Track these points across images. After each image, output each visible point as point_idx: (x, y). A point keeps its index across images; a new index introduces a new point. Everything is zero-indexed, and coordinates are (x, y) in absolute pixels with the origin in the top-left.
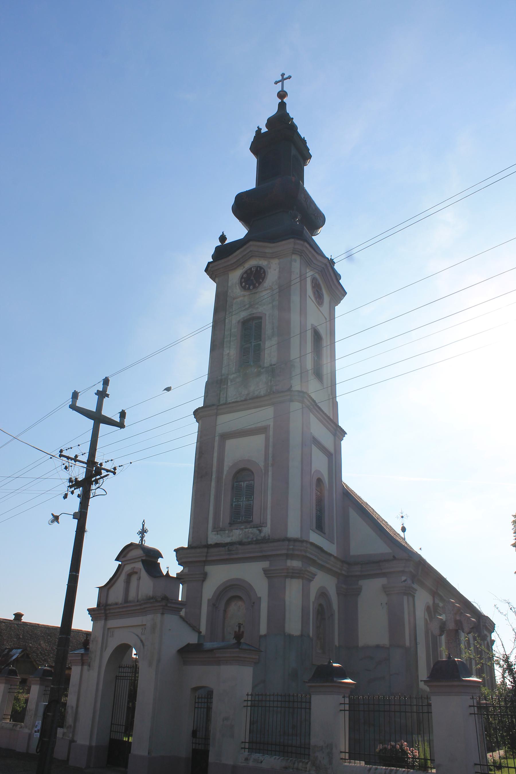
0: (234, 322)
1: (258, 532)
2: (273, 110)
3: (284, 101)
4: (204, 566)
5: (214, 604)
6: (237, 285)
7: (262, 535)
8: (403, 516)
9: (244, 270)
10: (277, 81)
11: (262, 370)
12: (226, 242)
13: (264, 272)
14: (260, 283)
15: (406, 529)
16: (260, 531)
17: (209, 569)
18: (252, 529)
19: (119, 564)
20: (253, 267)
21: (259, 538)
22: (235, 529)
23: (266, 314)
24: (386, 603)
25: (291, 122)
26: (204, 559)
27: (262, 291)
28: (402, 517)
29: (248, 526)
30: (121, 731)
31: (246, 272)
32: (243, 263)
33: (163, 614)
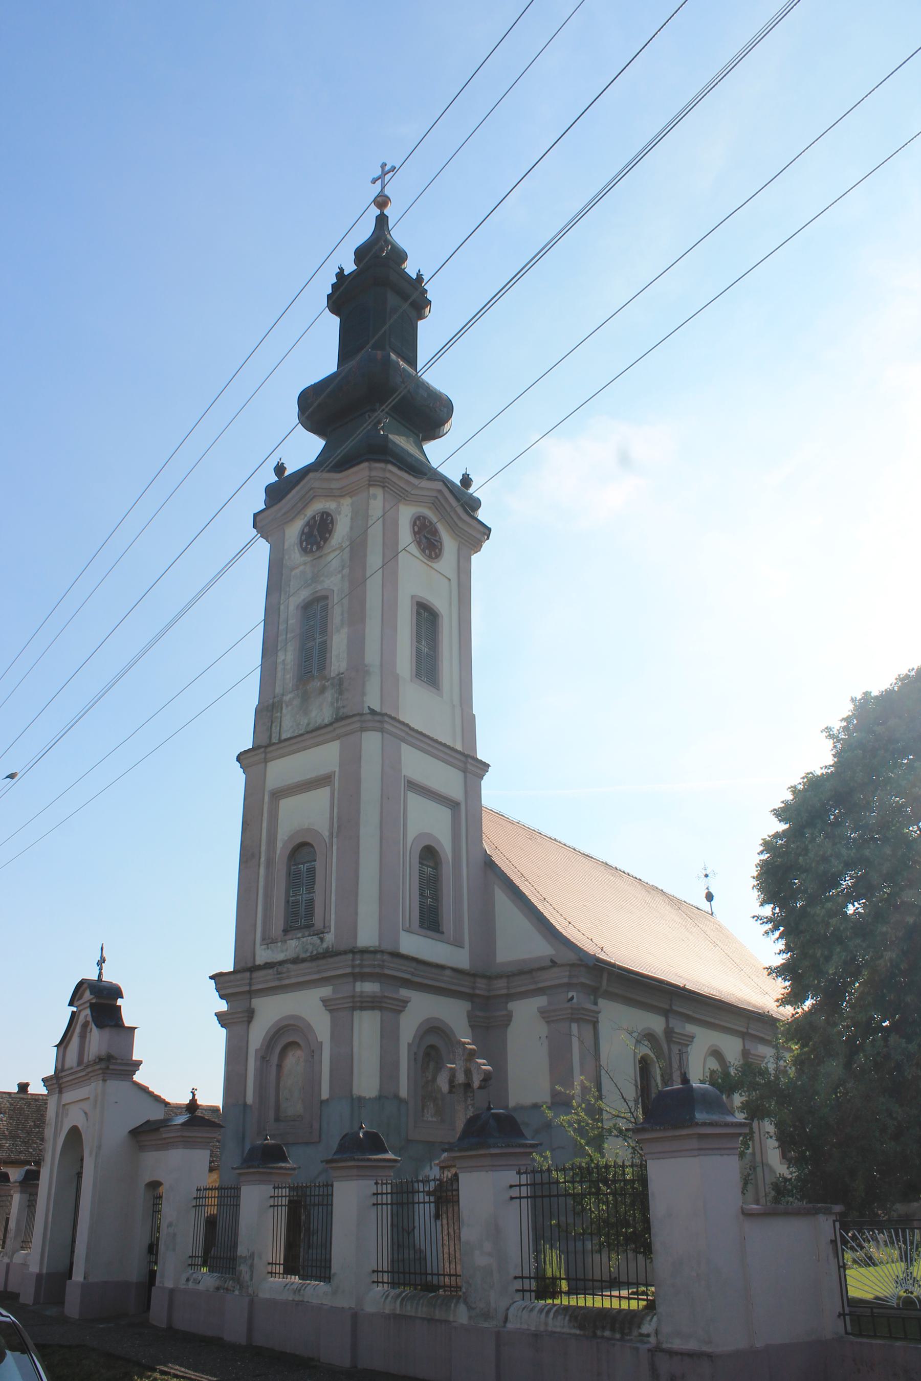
0: (292, 608)
1: (318, 941)
2: (365, 231)
3: (385, 213)
4: (251, 999)
5: (263, 1058)
6: (296, 546)
7: (325, 945)
8: (708, 873)
9: (306, 519)
10: (375, 177)
11: (327, 684)
12: (287, 474)
13: (332, 522)
14: (326, 540)
15: (713, 896)
16: (322, 940)
17: (257, 1003)
18: (311, 937)
19: (73, 1012)
20: (317, 514)
21: (321, 951)
22: (289, 940)
23: (334, 591)
24: (547, 1037)
25: (385, 252)
26: (247, 988)
27: (329, 553)
28: (706, 876)
29: (307, 933)
30: (412, 1271)
31: (308, 524)
32: (303, 508)
33: (104, 1080)
